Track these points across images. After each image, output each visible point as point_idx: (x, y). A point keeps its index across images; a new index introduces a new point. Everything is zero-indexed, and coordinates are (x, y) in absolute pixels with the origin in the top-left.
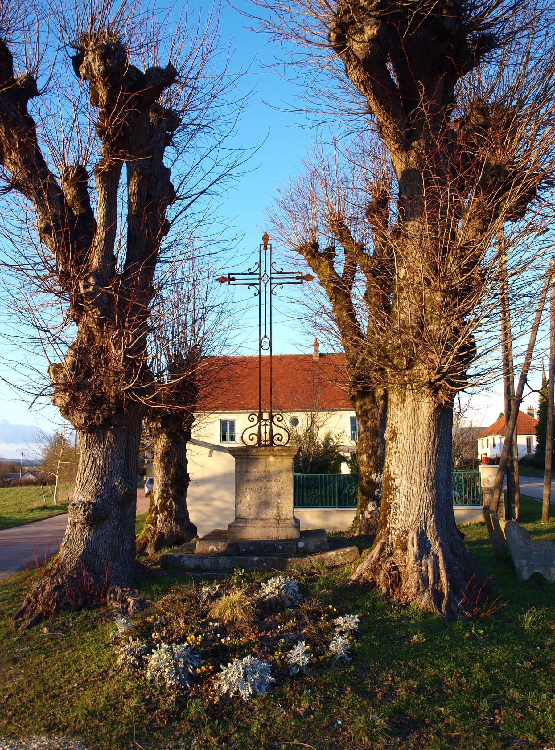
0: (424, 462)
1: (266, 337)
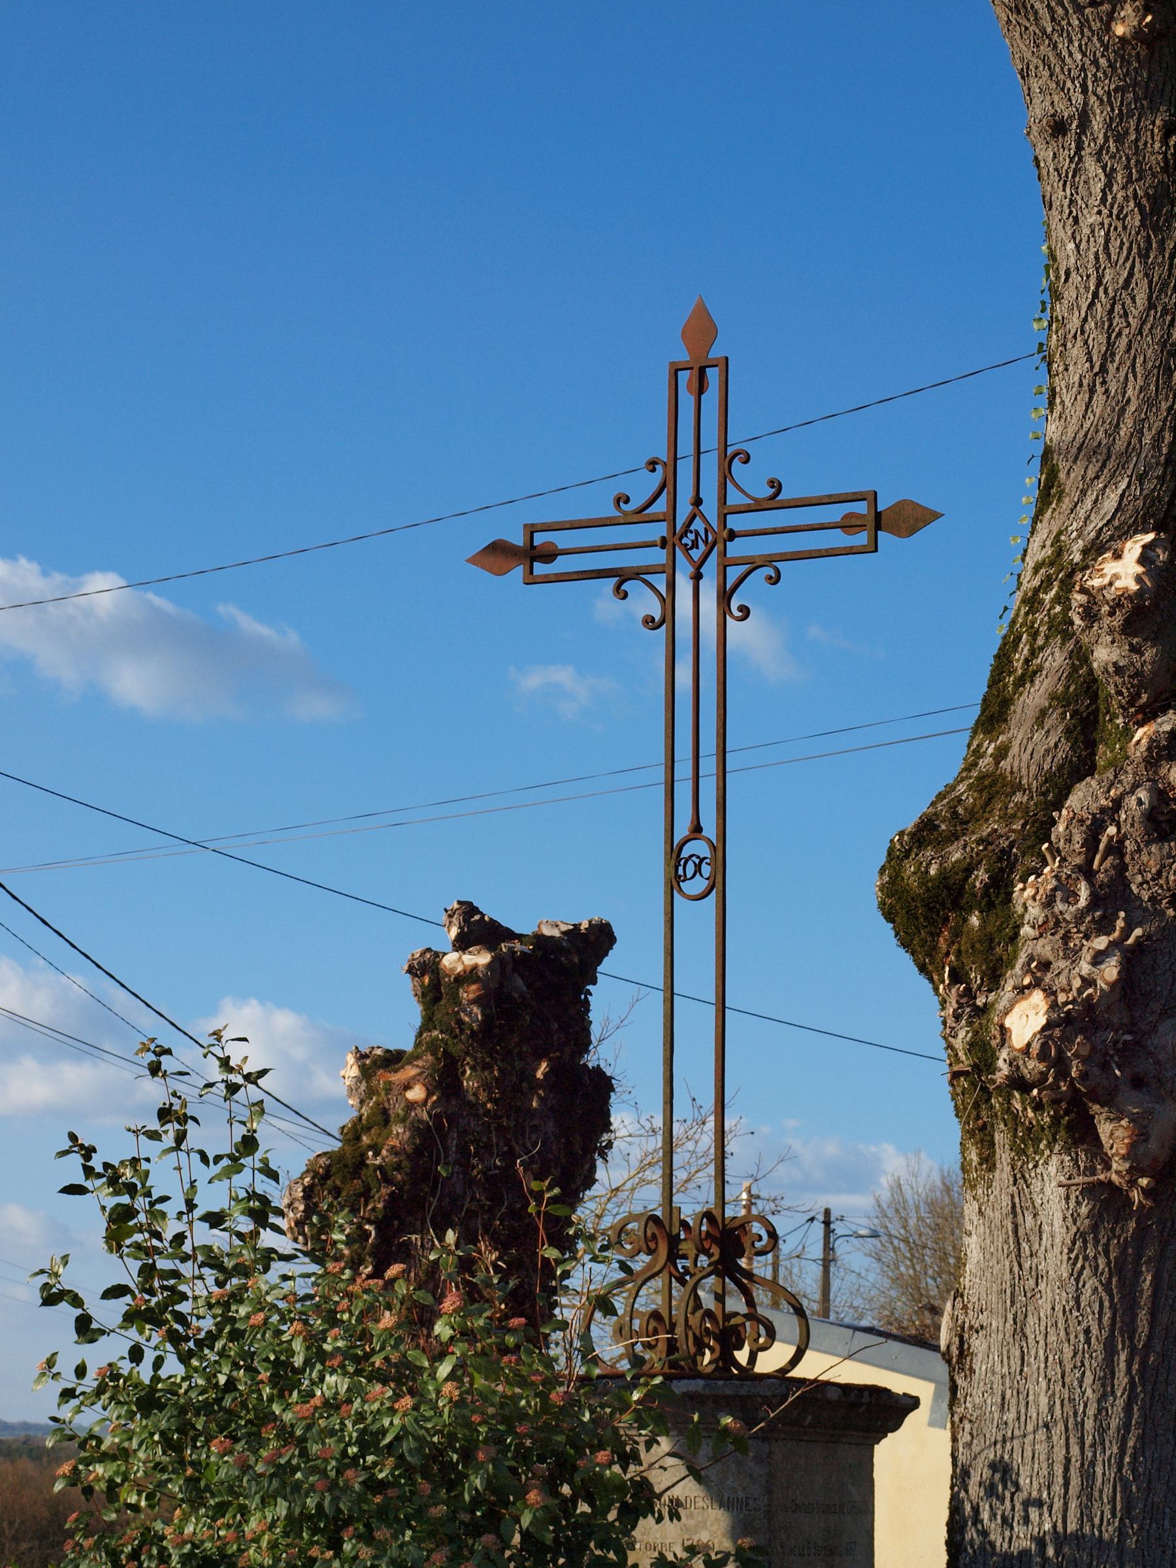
0: (1059, 1470)
1: (697, 829)
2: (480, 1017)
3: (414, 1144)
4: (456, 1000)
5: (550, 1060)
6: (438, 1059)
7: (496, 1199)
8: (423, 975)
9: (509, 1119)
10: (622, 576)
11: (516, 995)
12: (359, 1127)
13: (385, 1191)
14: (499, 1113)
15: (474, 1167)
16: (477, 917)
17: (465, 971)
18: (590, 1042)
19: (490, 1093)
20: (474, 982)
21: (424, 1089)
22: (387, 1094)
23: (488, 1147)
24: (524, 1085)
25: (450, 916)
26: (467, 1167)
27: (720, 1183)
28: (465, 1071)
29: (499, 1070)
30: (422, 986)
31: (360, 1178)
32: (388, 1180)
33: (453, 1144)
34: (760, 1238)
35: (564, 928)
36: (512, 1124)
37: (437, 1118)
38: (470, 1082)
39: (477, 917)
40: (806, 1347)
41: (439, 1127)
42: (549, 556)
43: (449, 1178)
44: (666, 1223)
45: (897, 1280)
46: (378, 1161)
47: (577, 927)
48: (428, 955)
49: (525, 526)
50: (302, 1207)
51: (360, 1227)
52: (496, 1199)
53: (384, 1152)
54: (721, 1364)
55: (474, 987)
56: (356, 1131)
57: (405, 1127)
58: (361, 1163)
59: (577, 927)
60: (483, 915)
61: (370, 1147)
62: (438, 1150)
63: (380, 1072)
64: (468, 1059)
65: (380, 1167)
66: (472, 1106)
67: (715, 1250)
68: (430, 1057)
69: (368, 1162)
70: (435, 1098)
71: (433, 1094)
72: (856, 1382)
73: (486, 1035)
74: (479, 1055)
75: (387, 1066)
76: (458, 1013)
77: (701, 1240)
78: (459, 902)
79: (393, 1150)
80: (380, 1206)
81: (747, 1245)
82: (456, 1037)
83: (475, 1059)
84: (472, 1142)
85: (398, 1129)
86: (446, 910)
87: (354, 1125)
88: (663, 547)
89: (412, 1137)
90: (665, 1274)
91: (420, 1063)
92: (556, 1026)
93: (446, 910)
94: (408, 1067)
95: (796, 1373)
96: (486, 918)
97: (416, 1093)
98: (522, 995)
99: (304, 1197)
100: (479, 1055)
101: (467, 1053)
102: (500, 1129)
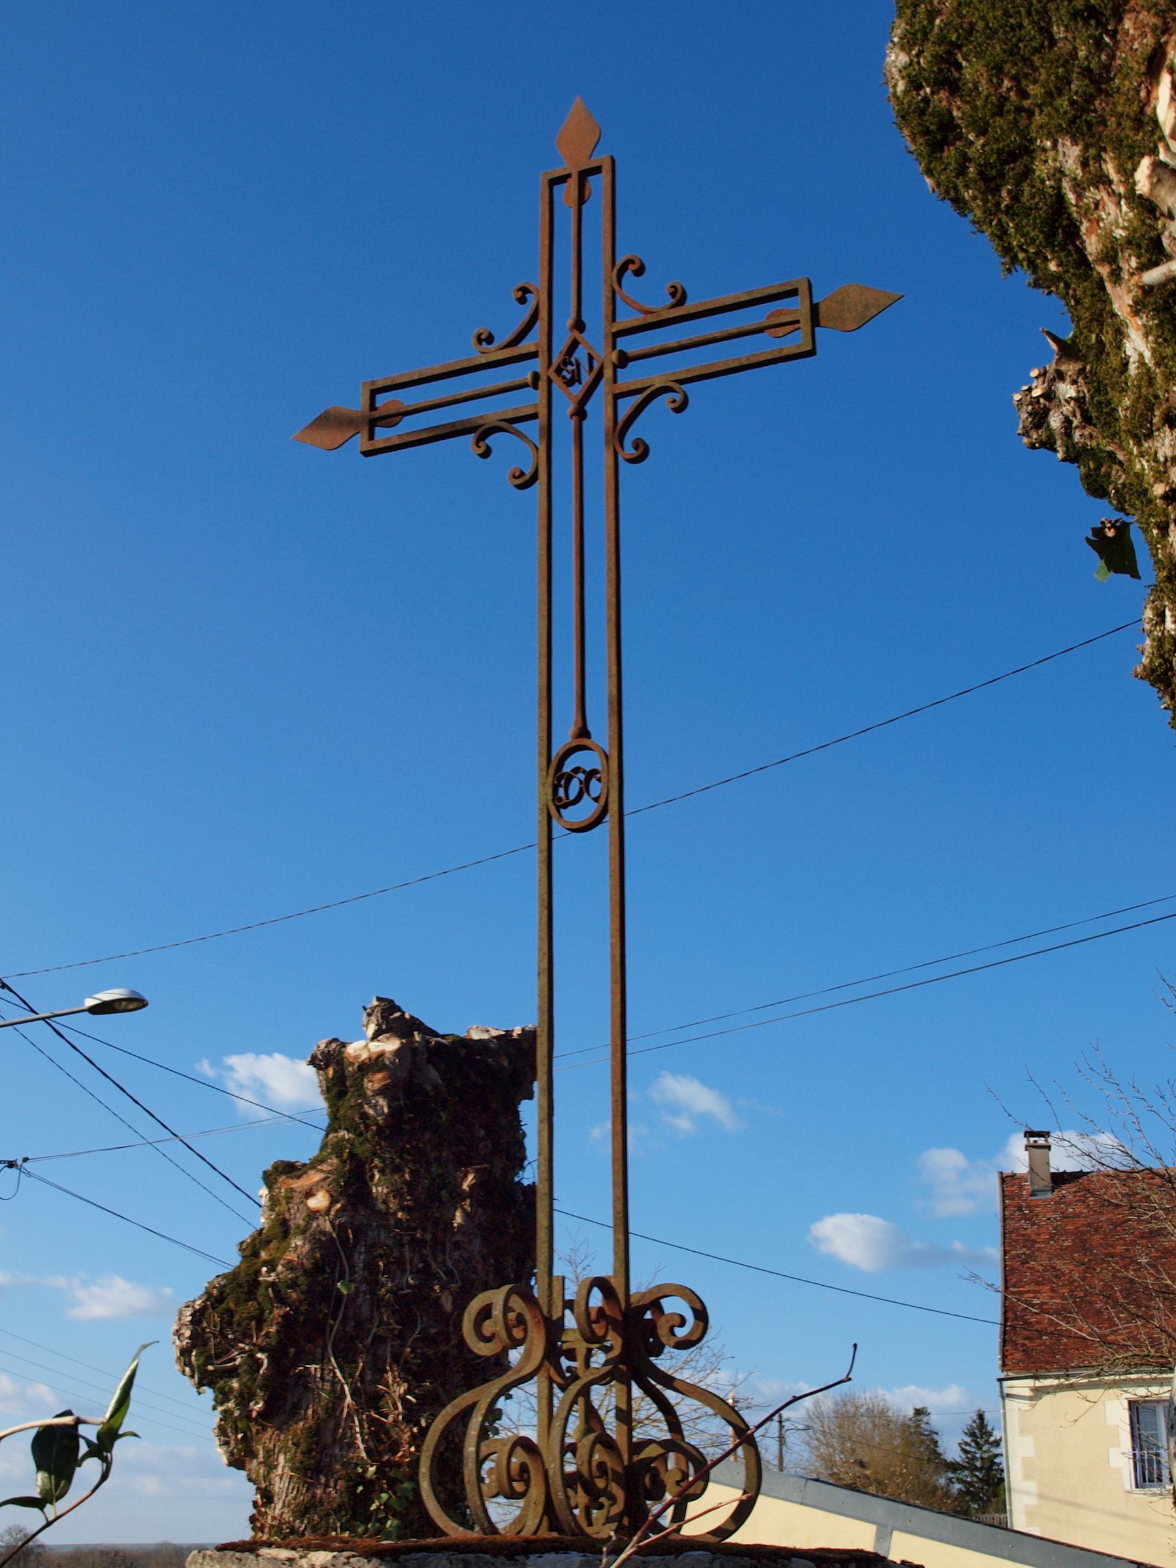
2: (386, 1110)
3: (314, 1258)
4: (360, 1089)
5: (477, 1171)
6: (344, 1162)
7: (407, 1322)
8: (327, 1066)
9: (424, 1230)
10: (483, 432)
11: (429, 1087)
12: (257, 1242)
13: (279, 1312)
14: (413, 1224)
15: (383, 1286)
16: (397, 1014)
17: (370, 1059)
18: (525, 1158)
19: (402, 1199)
20: (379, 1071)
21: (327, 1195)
22: (288, 1203)
23: (400, 1262)
24: (443, 1193)
25: (369, 1015)
26: (374, 1285)
27: (621, 1237)
28: (373, 1176)
29: (412, 1172)
30: (327, 1079)
31: (255, 1299)
32: (281, 1299)
33: (360, 1259)
34: (682, 1322)
35: (494, 1033)
36: (428, 1237)
37: (341, 1229)
38: (379, 1189)
39: (397, 1014)
40: (757, 1493)
41: (343, 1238)
42: (392, 419)
43: (352, 1298)
44: (543, 1302)
45: (820, 1457)
46: (272, 1277)
47: (509, 1033)
48: (334, 1045)
49: (365, 383)
50: (188, 1333)
51: (251, 1355)
52: (407, 1322)
53: (280, 1268)
54: (626, 1521)
55: (379, 1076)
56: (255, 1245)
57: (305, 1239)
58: (254, 1283)
59: (509, 1033)
60: (403, 1013)
61: (265, 1263)
62: (342, 1265)
63: (282, 1179)
64: (376, 1161)
65: (273, 1285)
66: (385, 1215)
67: (614, 1340)
68: (335, 1161)
69: (261, 1279)
70: (339, 1206)
71: (338, 1202)
72: (833, 1547)
73: (393, 1130)
74: (387, 1156)
75: (289, 1172)
76: (361, 1105)
77: (590, 1322)
78: (379, 999)
79: (290, 1266)
80: (273, 1329)
81: (662, 1332)
82: (361, 1134)
83: (384, 1161)
84: (381, 1256)
85: (297, 1241)
86: (365, 1009)
87: (254, 1239)
88: (536, 387)
89: (312, 1250)
90: (542, 1375)
91: (325, 1167)
92: (482, 1133)
93: (365, 1009)
94: (312, 1172)
95: (742, 1537)
96: (407, 1016)
97: (319, 1201)
98: (435, 1088)
99: (191, 1322)
100: (387, 1156)
101: (375, 1154)
102: (416, 1244)
